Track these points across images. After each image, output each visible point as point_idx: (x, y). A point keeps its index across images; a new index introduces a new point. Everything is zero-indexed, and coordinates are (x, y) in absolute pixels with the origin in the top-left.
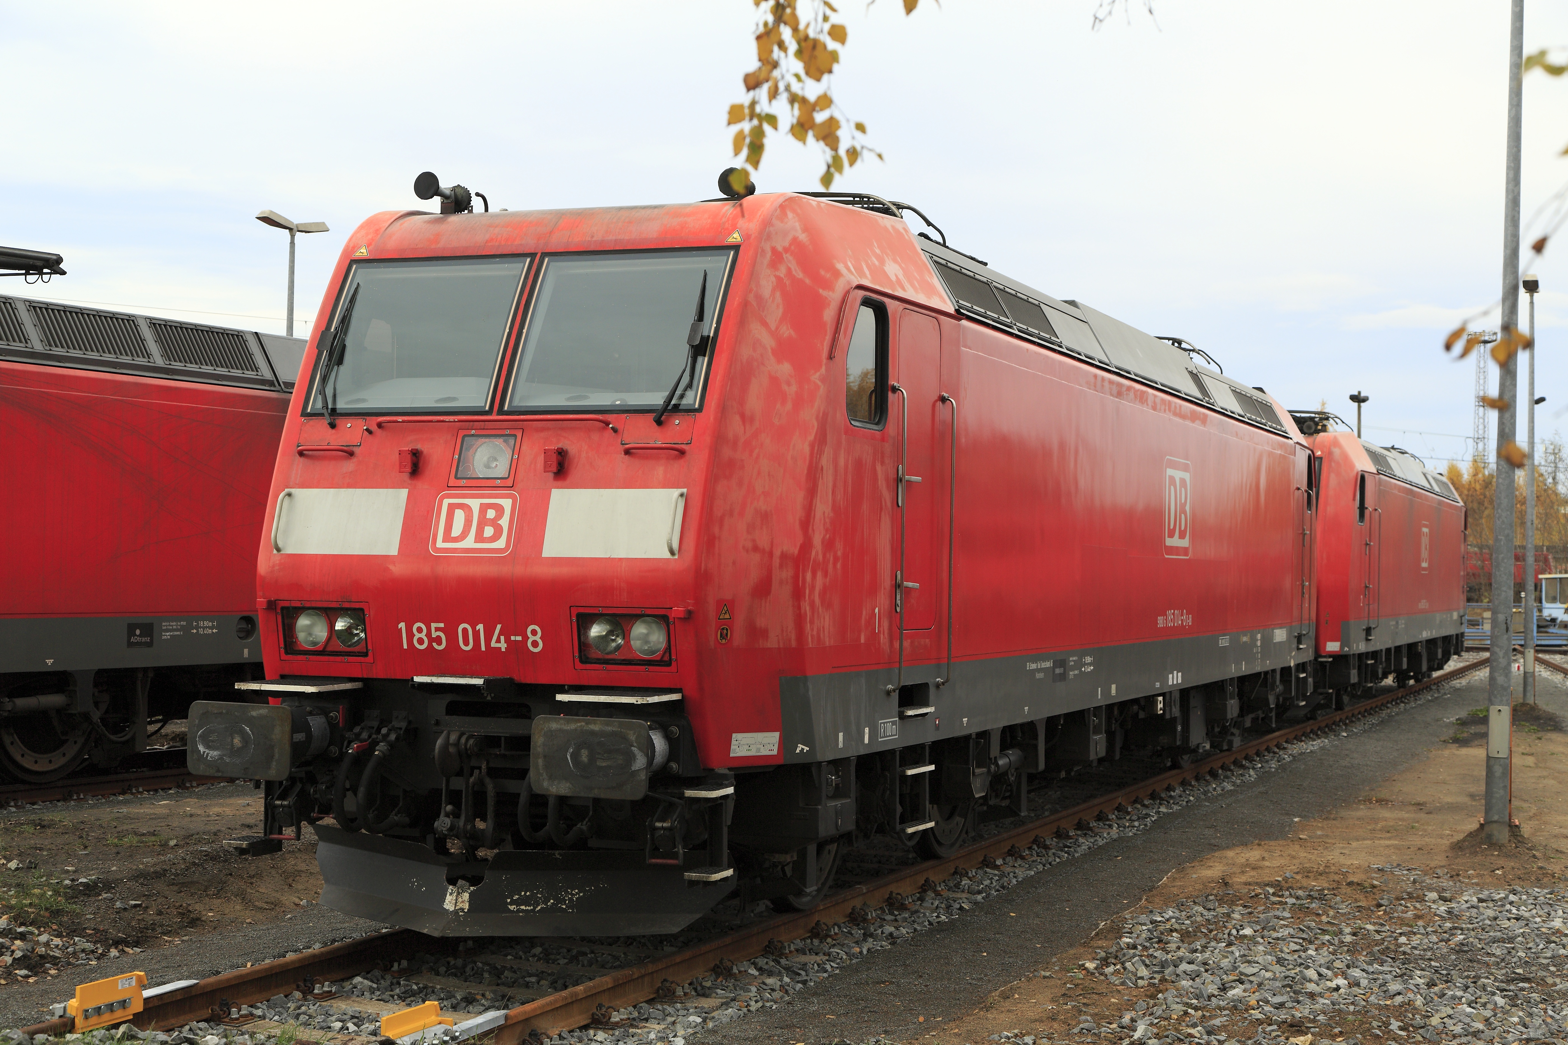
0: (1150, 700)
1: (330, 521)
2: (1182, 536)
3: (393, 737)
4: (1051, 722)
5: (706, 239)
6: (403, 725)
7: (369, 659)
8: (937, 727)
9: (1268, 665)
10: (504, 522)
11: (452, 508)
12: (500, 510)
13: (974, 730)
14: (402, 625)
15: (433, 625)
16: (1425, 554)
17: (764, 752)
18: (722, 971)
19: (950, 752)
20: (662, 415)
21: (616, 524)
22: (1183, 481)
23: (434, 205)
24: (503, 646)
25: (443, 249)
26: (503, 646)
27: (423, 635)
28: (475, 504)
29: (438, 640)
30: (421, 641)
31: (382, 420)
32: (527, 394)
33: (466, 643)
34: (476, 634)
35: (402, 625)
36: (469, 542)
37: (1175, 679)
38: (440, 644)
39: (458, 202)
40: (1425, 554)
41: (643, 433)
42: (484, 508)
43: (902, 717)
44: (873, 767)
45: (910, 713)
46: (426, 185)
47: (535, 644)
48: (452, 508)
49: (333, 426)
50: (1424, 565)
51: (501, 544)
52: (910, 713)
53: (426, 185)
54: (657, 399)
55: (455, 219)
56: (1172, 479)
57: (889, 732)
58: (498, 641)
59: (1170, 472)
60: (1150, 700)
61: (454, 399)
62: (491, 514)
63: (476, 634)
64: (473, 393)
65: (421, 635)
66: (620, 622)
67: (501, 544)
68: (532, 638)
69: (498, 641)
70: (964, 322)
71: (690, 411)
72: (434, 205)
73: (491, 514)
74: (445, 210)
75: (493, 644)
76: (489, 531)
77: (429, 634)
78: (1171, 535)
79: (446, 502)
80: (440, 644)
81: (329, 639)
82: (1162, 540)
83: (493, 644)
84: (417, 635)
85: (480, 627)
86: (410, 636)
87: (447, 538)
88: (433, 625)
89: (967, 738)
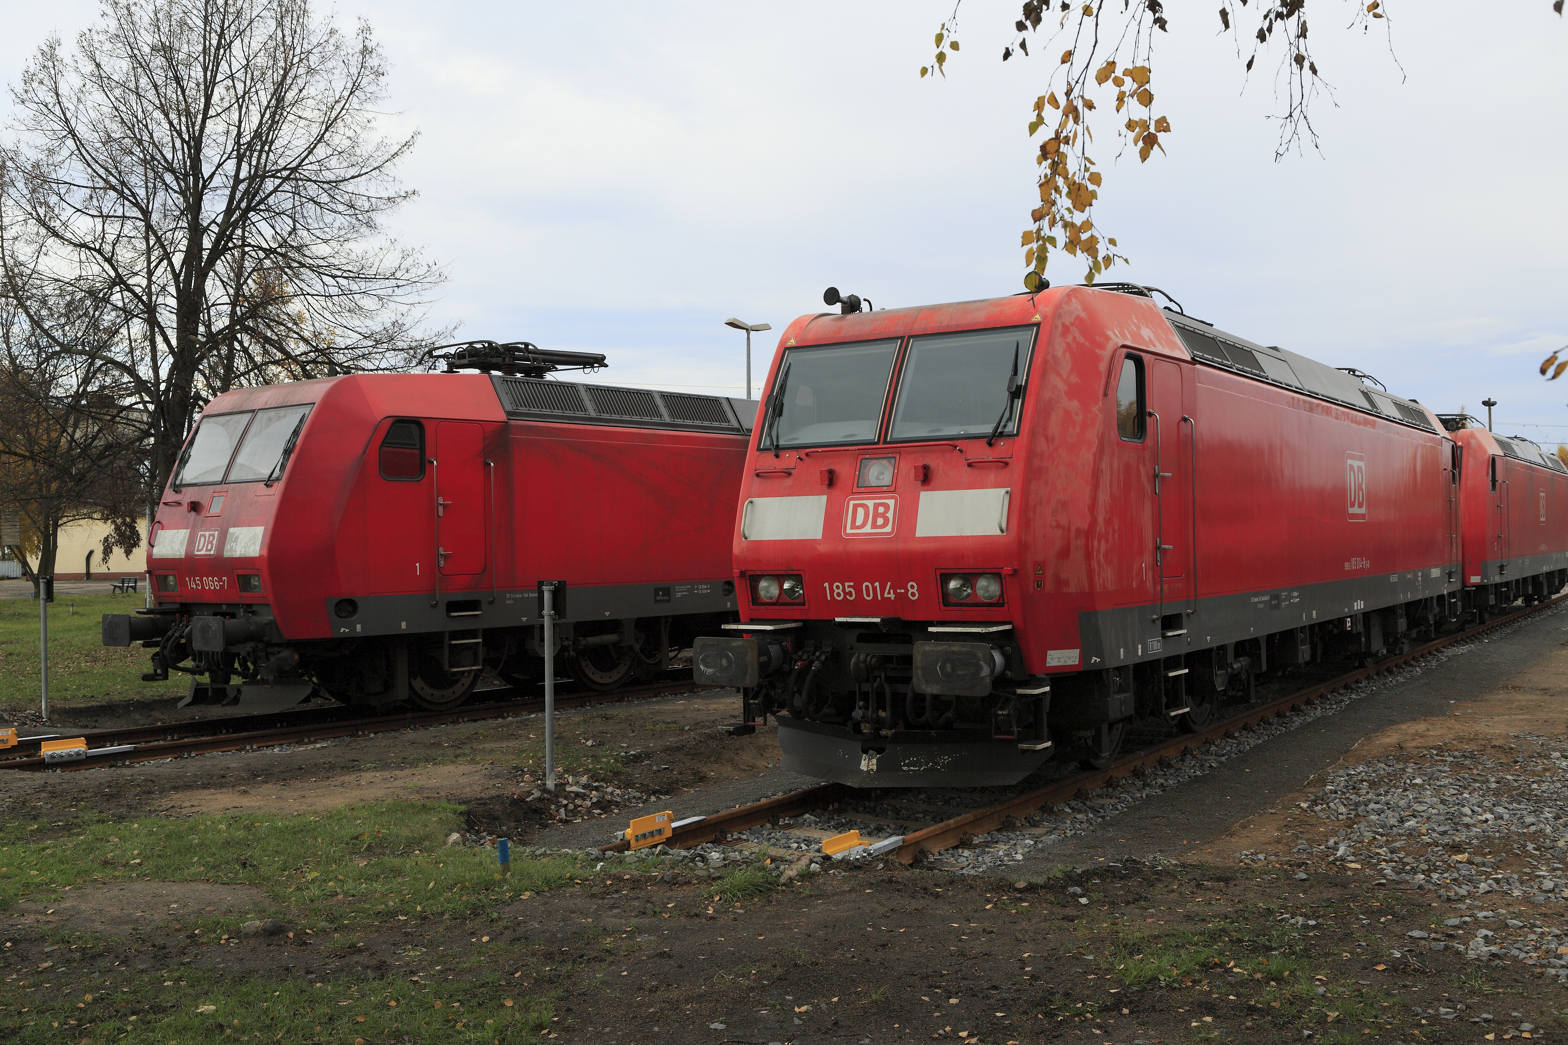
0: (1341, 621)
1: (778, 519)
2: (1360, 506)
3: (823, 658)
4: (1270, 637)
5: (1017, 320)
6: (830, 649)
7: (806, 607)
8: (1189, 643)
9: (1427, 594)
10: (890, 515)
11: (856, 507)
12: (887, 507)
13: (1214, 645)
14: (826, 584)
15: (847, 584)
16: (1542, 511)
17: (1070, 663)
18: (1047, 810)
19: (1199, 660)
20: (992, 439)
21: (967, 513)
22: (1360, 468)
23: (837, 308)
24: (892, 596)
25: (845, 342)
26: (892, 596)
27: (840, 591)
28: (870, 503)
29: (850, 594)
30: (839, 595)
31: (808, 451)
32: (902, 430)
33: (868, 595)
34: (875, 589)
35: (826, 584)
36: (868, 529)
37: (1359, 605)
38: (851, 595)
39: (852, 305)
40: (1542, 511)
41: (979, 452)
42: (876, 506)
43: (1164, 637)
44: (1146, 672)
45: (1170, 634)
46: (831, 296)
47: (913, 594)
48: (856, 507)
49: (777, 456)
50: (1543, 519)
51: (888, 529)
52: (1170, 634)
53: (831, 296)
54: (988, 429)
55: (851, 317)
56: (1352, 467)
57: (1155, 647)
58: (889, 593)
59: (1350, 462)
60: (1341, 621)
61: (855, 435)
62: (881, 510)
63: (875, 589)
64: (866, 431)
65: (839, 590)
66: (969, 578)
67: (888, 529)
68: (911, 591)
69: (889, 593)
70: (1198, 366)
71: (1011, 435)
72: (837, 308)
73: (881, 510)
74: (844, 311)
75: (886, 595)
76: (880, 521)
77: (844, 590)
78: (1352, 506)
79: (852, 503)
80: (851, 595)
81: (780, 594)
82: (1345, 509)
83: (886, 595)
84: (837, 591)
85: (877, 584)
86: (832, 591)
87: (853, 526)
88: (847, 584)
89: (1210, 650)
